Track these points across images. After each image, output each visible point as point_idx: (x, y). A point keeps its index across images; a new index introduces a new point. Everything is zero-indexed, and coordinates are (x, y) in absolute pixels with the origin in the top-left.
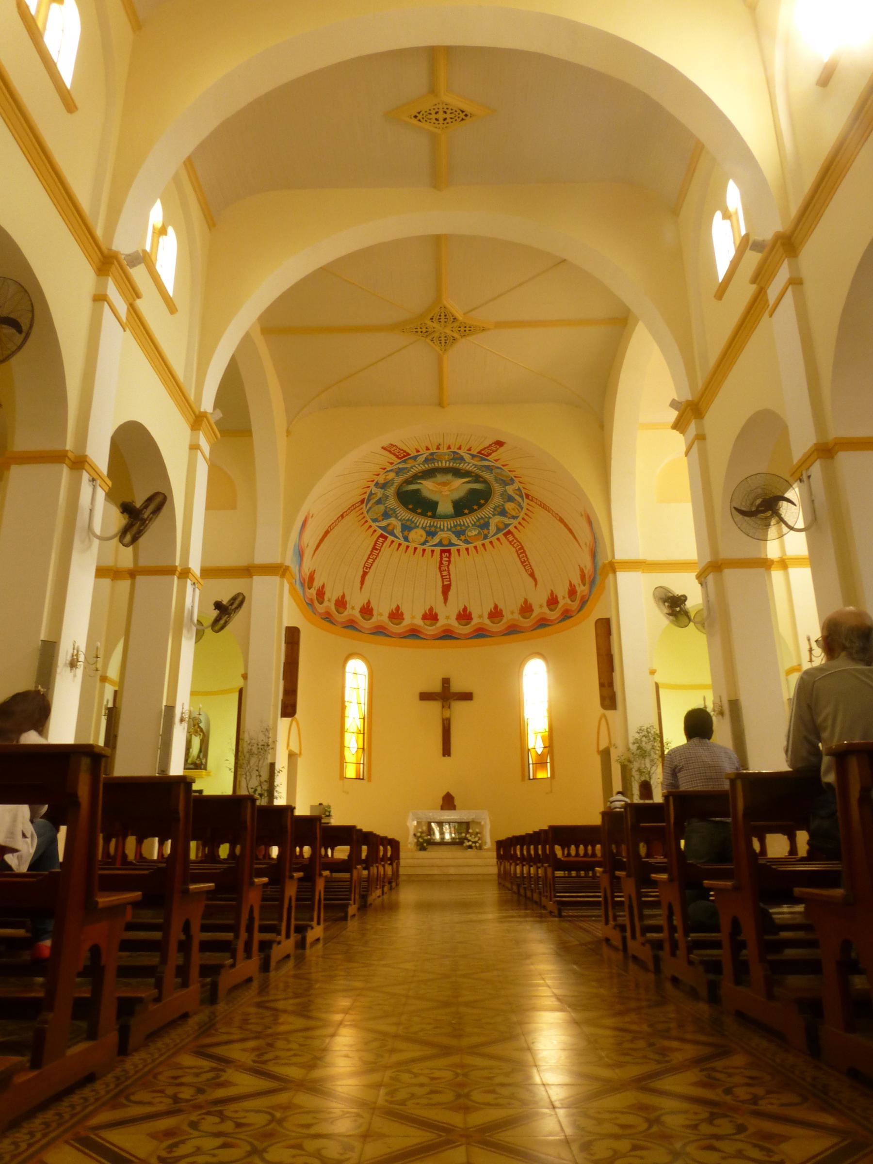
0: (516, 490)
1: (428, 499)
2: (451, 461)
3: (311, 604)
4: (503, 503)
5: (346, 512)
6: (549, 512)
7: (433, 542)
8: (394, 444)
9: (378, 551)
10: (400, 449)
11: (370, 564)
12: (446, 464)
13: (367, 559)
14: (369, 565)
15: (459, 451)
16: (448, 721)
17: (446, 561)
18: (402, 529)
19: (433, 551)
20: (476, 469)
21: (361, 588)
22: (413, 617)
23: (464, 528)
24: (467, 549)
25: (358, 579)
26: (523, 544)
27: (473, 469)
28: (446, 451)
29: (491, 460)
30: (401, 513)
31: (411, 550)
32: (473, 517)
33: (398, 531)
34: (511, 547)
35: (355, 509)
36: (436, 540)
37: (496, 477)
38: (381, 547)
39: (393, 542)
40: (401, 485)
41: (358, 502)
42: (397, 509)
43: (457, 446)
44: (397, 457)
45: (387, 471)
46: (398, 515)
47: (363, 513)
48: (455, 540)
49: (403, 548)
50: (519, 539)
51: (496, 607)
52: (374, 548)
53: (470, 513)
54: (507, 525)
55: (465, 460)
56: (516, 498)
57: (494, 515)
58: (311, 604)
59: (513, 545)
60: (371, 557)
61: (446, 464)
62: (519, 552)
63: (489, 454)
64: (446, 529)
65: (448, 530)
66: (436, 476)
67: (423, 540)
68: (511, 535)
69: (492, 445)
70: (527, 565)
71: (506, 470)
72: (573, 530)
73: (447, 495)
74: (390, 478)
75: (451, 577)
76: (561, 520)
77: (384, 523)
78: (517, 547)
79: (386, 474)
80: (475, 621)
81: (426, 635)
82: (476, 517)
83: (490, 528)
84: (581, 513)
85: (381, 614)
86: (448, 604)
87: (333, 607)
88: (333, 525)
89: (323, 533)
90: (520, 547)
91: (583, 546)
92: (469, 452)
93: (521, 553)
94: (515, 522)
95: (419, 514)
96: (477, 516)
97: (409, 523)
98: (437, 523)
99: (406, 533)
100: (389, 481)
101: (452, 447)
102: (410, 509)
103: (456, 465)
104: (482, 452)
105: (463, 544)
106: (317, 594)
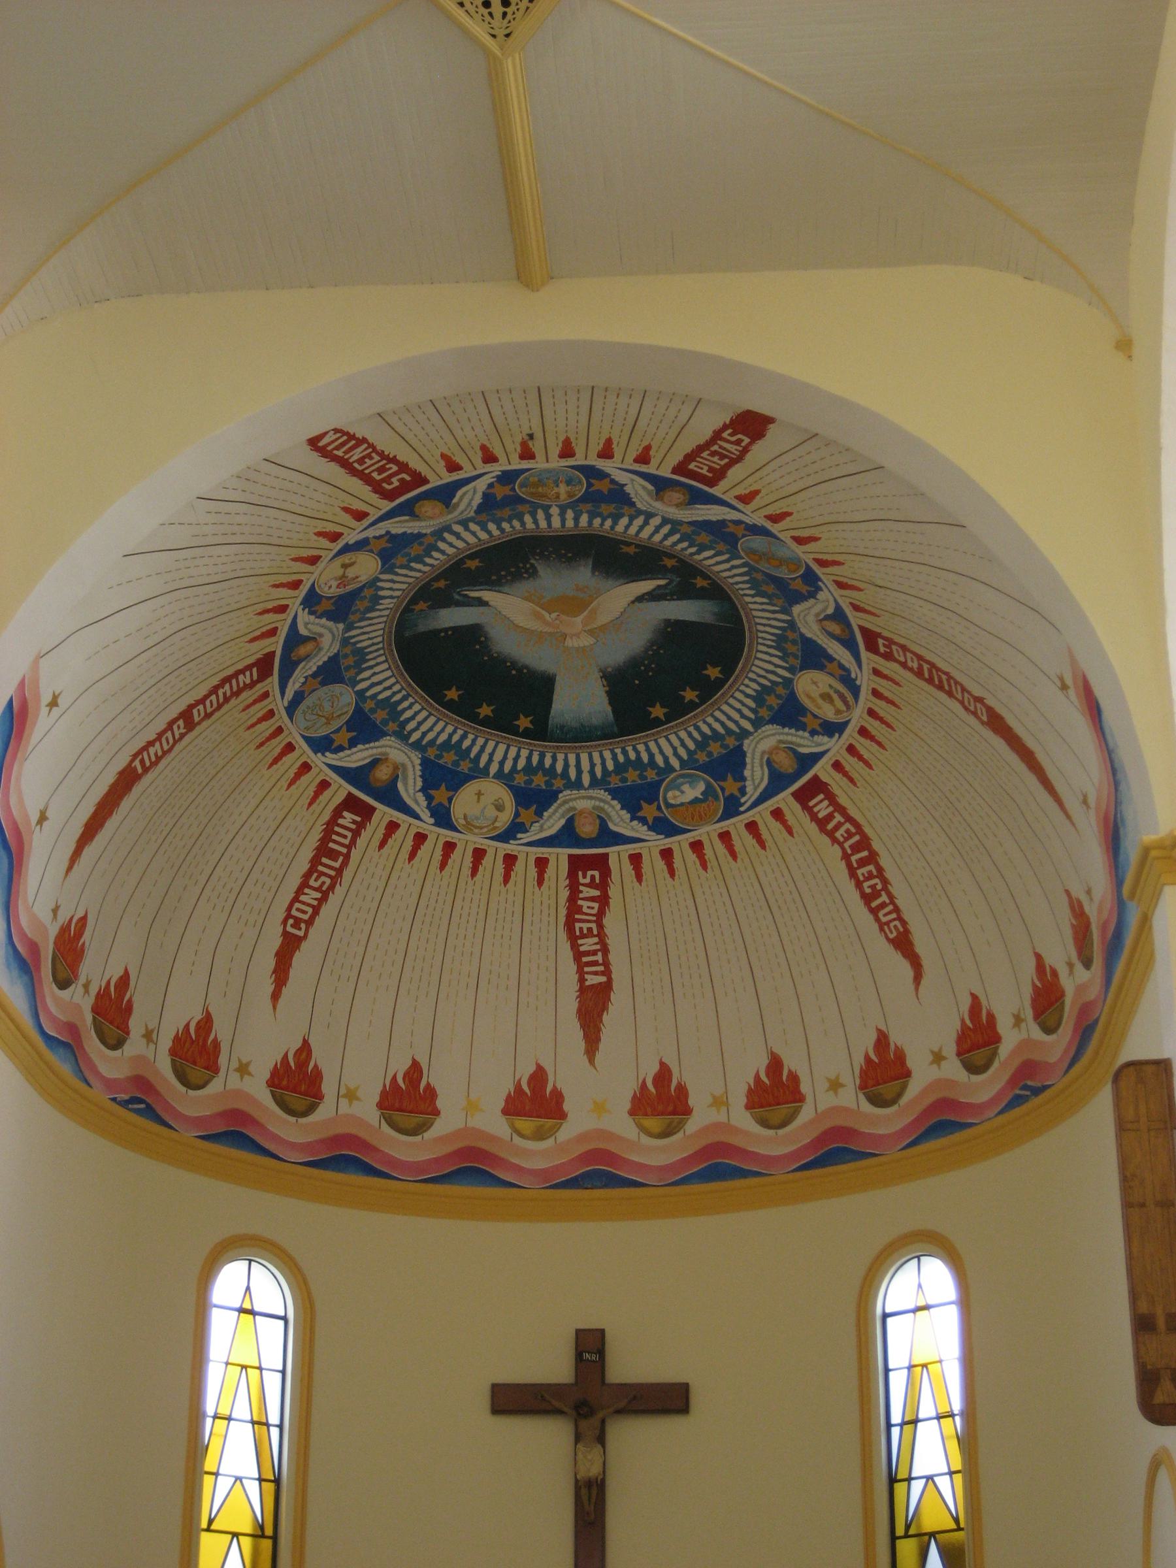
0: (827, 618)
1: (514, 664)
2: (581, 506)
3: (65, 1045)
4: (787, 675)
5: (202, 701)
6: (950, 694)
7: (542, 829)
8: (359, 435)
9: (341, 858)
10: (382, 455)
11: (310, 910)
12: (563, 521)
13: (300, 891)
14: (305, 912)
15: (602, 464)
16: (594, 1491)
17: (592, 899)
18: (425, 781)
19: (542, 863)
20: (677, 536)
21: (276, 996)
22: (471, 1107)
23: (651, 775)
24: (667, 854)
25: (267, 962)
26: (867, 830)
27: (666, 537)
28: (556, 463)
29: (724, 497)
30: (419, 718)
31: (461, 858)
32: (683, 734)
33: (410, 789)
34: (827, 840)
35: (237, 694)
36: (553, 822)
37: (752, 569)
38: (349, 847)
39: (392, 827)
40: (407, 610)
41: (249, 667)
42: (406, 704)
43: (596, 446)
44: (377, 488)
45: (347, 549)
46: (411, 726)
47: (271, 714)
48: (620, 821)
49: (431, 850)
50: (853, 812)
51: (775, 1064)
52: (323, 850)
53: (669, 718)
54: (807, 761)
55: (633, 504)
56: (830, 651)
57: (757, 723)
58: (65, 1045)
59: (831, 835)
60: (312, 883)
61: (563, 521)
62: (854, 858)
63: (718, 475)
64: (586, 779)
65: (595, 783)
66: (533, 573)
67: (505, 819)
68: (821, 796)
69: (725, 435)
70: (883, 905)
71: (785, 537)
72: (1041, 756)
73: (582, 650)
74: (364, 579)
75: (612, 957)
76: (996, 723)
77: (357, 757)
78: (846, 839)
79: (346, 558)
80: (701, 1117)
81: (519, 1169)
82: (696, 735)
83: (747, 773)
84: (1061, 679)
85: (351, 1096)
86: (599, 1057)
87: (164, 1065)
88: (152, 750)
89: (109, 778)
90: (857, 838)
91: (1073, 805)
92: (643, 468)
93: (862, 863)
94: (835, 747)
95: (486, 722)
96: (697, 728)
97: (448, 759)
98: (554, 759)
99: (440, 795)
100: (361, 589)
101: (579, 450)
102: (450, 706)
103: (602, 526)
104: (692, 466)
105: (652, 835)
106: (96, 1010)
